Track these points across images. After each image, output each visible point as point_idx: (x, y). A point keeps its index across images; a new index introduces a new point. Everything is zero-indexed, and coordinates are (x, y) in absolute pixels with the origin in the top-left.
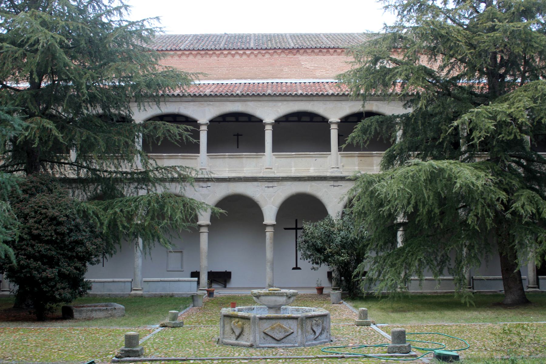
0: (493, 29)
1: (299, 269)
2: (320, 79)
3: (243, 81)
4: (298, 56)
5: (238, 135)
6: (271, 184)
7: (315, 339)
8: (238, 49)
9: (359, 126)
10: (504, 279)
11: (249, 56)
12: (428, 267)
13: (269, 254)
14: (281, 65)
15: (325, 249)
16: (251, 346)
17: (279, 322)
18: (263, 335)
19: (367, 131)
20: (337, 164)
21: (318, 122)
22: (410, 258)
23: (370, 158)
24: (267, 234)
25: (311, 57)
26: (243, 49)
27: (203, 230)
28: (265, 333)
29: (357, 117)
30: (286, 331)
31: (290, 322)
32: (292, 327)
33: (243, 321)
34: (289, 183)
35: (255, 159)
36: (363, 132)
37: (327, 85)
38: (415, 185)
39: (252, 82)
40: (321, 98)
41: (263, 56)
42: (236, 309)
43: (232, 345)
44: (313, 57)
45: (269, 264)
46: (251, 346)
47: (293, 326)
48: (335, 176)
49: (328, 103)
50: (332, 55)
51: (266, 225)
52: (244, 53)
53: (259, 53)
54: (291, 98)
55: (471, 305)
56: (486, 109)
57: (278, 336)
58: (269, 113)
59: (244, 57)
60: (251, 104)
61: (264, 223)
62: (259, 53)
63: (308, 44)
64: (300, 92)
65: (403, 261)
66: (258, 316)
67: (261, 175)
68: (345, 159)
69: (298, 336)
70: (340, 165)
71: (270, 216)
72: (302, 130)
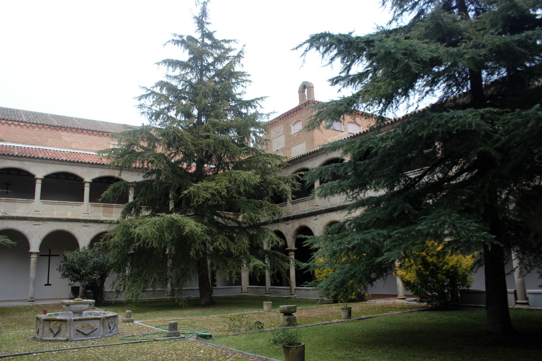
0: (208, 137)
1: (50, 285)
2: (75, 150)
3: (16, 145)
4: (60, 132)
5: (8, 184)
6: (37, 223)
7: (110, 332)
8: (15, 121)
9: (112, 187)
10: (200, 289)
11: (22, 127)
12: (159, 282)
13: (32, 274)
14: (47, 137)
15: (81, 271)
16: (67, 340)
17: (87, 322)
18: (76, 332)
19: (117, 190)
20: (88, 211)
21: (78, 181)
22: (147, 277)
23: (111, 208)
24: (32, 259)
25: (70, 134)
26: (18, 121)
27: (33, 256)
28: (77, 330)
29: (110, 180)
30: (92, 328)
31: (95, 321)
32: (96, 325)
33: (61, 323)
34: (52, 222)
35: (26, 204)
36: (105, 189)
37: (73, 154)
38: (161, 230)
39: (23, 146)
40: (80, 164)
41: (34, 128)
42: (48, 314)
43: (50, 341)
44: (71, 134)
45: (32, 282)
46: (67, 340)
47: (97, 324)
48: (86, 220)
49: (84, 168)
50: (85, 134)
51: (32, 253)
52: (19, 124)
53: (31, 126)
54: (58, 162)
55: (185, 306)
56: (202, 185)
57: (86, 332)
58: (40, 172)
59: (19, 127)
60: (27, 163)
61: (30, 251)
62: (25, 125)
63: (66, 124)
64: (16, 153)
65: (143, 279)
66: (73, 318)
67: (30, 216)
68: (93, 208)
69: (101, 331)
70: (90, 212)
71: (35, 247)
72: (64, 186)
